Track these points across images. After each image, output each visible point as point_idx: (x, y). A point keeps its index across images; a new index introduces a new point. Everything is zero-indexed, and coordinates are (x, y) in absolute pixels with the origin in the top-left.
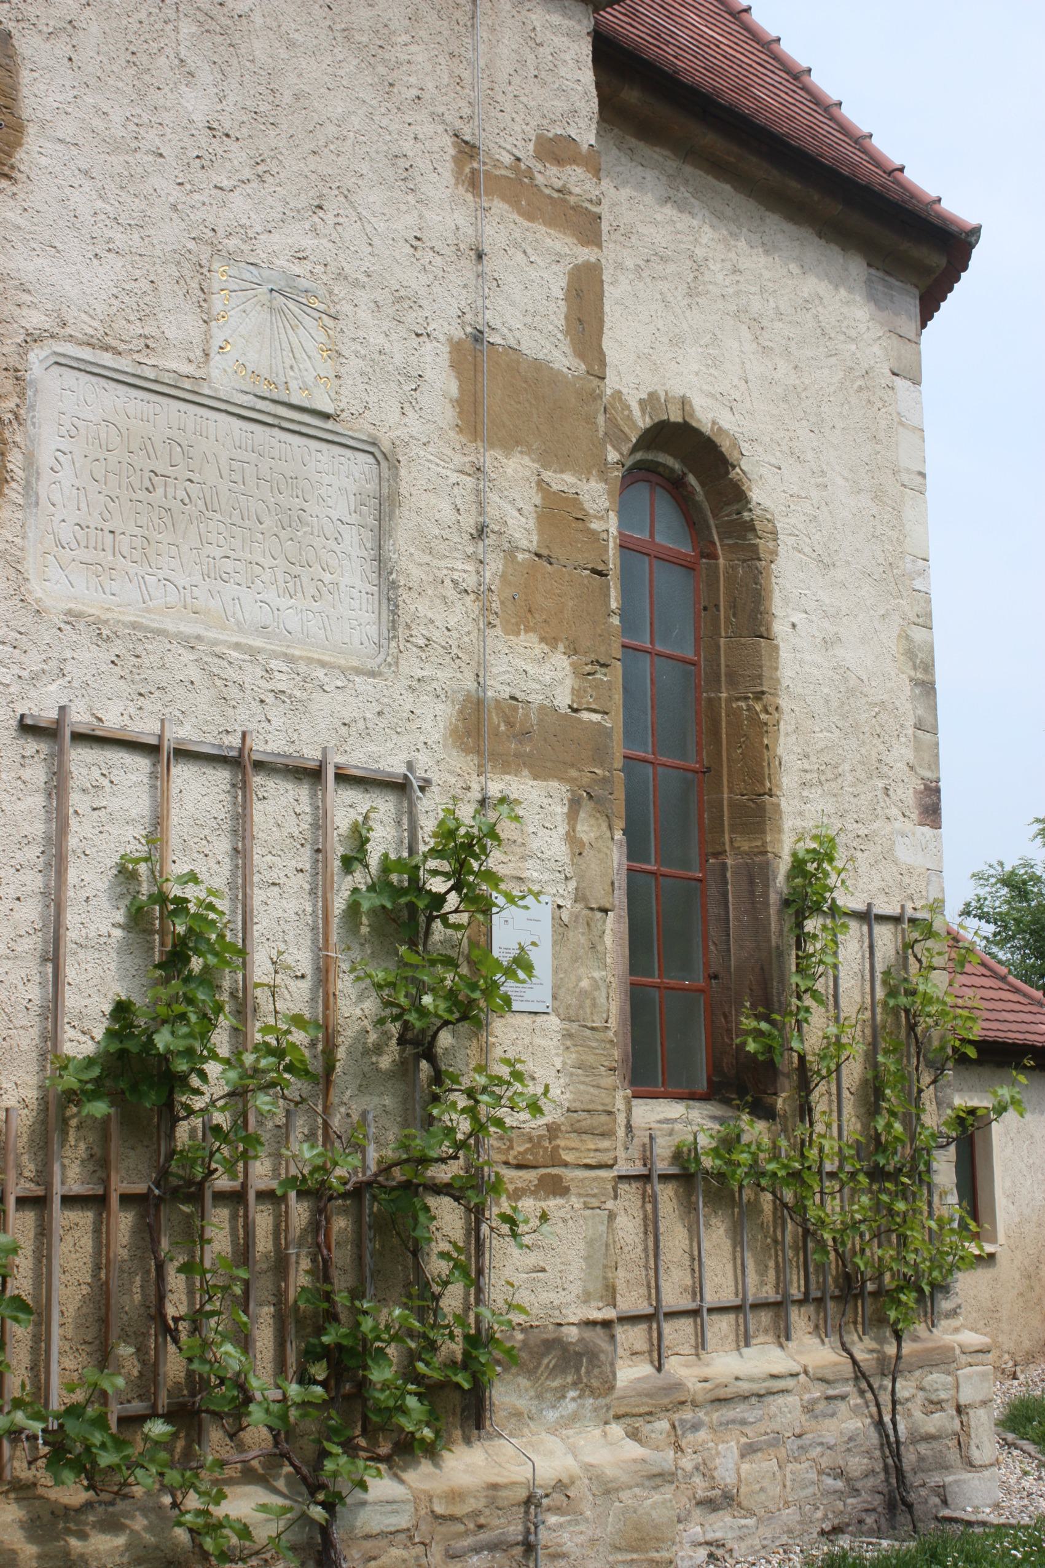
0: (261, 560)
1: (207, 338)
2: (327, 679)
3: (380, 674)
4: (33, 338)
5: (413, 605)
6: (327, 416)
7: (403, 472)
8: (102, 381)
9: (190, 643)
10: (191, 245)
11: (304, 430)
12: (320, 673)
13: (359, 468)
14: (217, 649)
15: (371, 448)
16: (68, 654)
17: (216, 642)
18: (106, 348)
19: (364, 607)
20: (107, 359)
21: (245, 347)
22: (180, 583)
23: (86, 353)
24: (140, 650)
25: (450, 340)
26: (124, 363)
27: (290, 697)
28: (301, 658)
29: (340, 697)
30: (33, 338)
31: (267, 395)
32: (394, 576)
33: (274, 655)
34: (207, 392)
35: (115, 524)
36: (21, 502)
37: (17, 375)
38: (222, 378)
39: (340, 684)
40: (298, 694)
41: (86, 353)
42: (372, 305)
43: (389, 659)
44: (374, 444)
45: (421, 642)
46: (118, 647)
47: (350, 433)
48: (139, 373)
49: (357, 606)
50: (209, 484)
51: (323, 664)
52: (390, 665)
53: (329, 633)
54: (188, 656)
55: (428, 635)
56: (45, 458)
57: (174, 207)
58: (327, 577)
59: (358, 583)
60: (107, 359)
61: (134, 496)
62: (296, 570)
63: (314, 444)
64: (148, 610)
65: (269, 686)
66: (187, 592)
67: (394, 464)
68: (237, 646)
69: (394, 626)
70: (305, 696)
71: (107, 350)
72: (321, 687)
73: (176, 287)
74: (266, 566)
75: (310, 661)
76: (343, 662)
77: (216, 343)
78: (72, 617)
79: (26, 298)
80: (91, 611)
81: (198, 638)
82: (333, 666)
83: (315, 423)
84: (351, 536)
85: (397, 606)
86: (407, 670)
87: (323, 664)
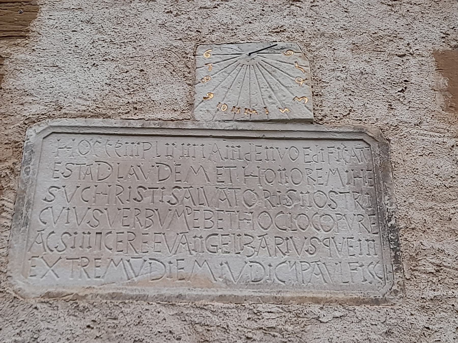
0: (249, 232)
1: (192, 94)
2: (322, 312)
3: (386, 301)
4: (30, 121)
5: (410, 242)
6: (310, 122)
7: (393, 147)
8: (96, 138)
9: (169, 302)
10: (178, 43)
11: (127, 132)
12: (315, 308)
13: (351, 155)
14: (198, 303)
15: (359, 135)
16: (43, 325)
17: (199, 298)
18: (97, 116)
19: (365, 252)
20: (98, 122)
21: (222, 91)
22: (166, 260)
23: (80, 122)
24: (116, 312)
25: (435, 53)
26: (115, 122)
27: (281, 331)
28: (292, 298)
29: (338, 325)
30: (30, 121)
31: (248, 118)
32: (393, 222)
33: (264, 300)
34: (190, 126)
35: (104, 227)
36: (9, 224)
37: (18, 147)
38: (203, 115)
39: (337, 314)
40: (290, 328)
41: (80, 122)
42: (351, 46)
43: (395, 288)
44: (361, 133)
45: (431, 269)
46: (95, 314)
47: (335, 130)
48: (127, 125)
49: (357, 252)
50: (195, 186)
51: (317, 301)
52: (396, 292)
53: (327, 277)
54: (167, 312)
55: (438, 262)
56: (41, 192)
57: (163, 25)
58: (322, 234)
59: (356, 234)
60: (98, 122)
61: (122, 206)
62: (289, 233)
63: (300, 145)
64: (133, 283)
65: (255, 325)
66: (174, 266)
67: (385, 145)
68: (221, 298)
69: (397, 259)
70: (298, 328)
71: (98, 117)
72: (318, 319)
73: (164, 70)
74: (256, 235)
75: (301, 300)
76: (341, 296)
77: (198, 98)
78: (50, 298)
79: (29, 99)
80: (69, 292)
81: (179, 296)
82: (329, 302)
83: (312, 129)
84: (346, 204)
85: (399, 245)
86: (417, 294)
87: (317, 301)
